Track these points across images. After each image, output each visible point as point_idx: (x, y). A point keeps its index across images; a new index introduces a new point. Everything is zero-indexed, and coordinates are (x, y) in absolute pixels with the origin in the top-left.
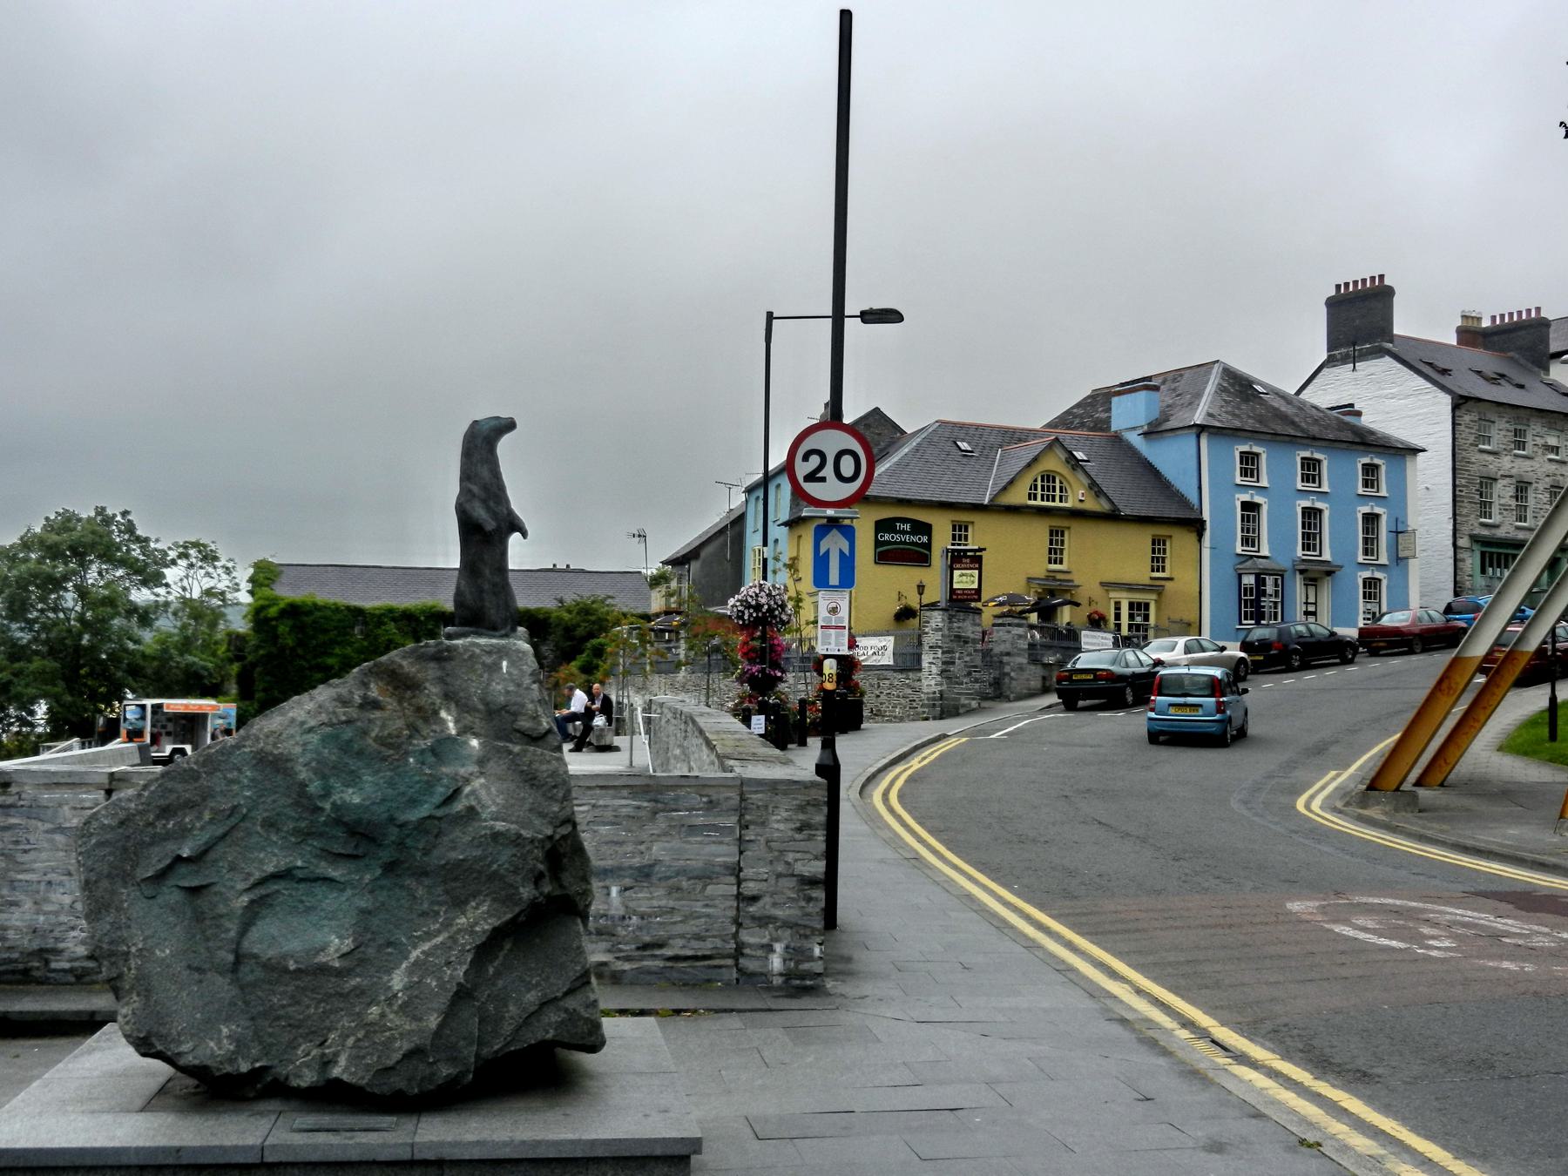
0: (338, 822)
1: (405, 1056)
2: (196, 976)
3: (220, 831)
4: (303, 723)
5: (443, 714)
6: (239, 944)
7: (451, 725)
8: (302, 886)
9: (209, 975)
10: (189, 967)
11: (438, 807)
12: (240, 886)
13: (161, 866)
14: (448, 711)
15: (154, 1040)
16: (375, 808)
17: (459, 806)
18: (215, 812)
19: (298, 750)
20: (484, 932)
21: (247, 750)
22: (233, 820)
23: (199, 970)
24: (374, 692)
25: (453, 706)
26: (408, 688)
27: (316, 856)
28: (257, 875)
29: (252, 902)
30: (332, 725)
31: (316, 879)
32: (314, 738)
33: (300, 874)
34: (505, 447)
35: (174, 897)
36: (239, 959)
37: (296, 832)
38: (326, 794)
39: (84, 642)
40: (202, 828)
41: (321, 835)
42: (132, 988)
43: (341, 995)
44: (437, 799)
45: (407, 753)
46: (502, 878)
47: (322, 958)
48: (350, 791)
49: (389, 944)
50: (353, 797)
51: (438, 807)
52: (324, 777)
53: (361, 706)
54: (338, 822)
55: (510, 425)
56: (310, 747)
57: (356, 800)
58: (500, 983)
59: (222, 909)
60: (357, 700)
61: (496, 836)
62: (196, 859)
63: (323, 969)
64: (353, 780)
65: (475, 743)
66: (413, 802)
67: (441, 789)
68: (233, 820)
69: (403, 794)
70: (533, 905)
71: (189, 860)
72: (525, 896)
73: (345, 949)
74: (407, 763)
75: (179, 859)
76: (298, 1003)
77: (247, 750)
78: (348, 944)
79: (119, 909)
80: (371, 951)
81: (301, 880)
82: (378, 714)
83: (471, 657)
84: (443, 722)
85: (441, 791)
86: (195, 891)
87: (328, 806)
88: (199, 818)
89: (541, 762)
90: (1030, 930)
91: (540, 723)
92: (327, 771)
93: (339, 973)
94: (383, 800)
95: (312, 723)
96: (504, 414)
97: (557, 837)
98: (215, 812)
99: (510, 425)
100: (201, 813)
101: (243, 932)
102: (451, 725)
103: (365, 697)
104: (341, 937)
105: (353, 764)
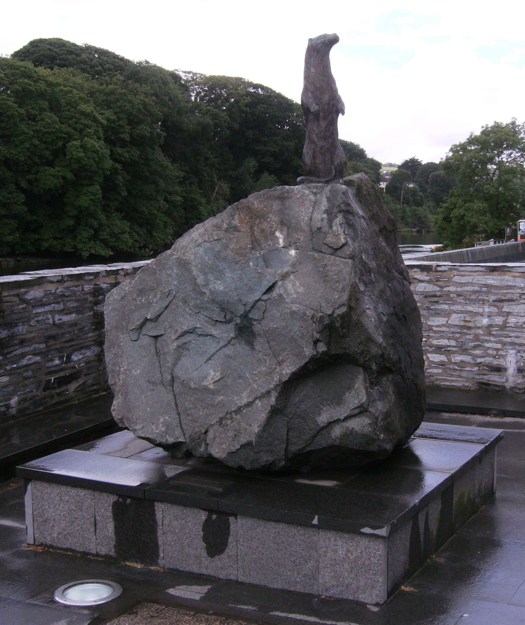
0: (213, 301)
1: (242, 446)
2: (151, 387)
3: (164, 306)
4: (196, 241)
5: (278, 234)
6: (173, 370)
7: (281, 241)
8: (201, 338)
9: (158, 387)
10: (149, 381)
11: (265, 293)
12: (174, 337)
13: (139, 323)
14: (281, 231)
15: (125, 421)
16: (230, 293)
17: (274, 294)
18: (163, 293)
19: (193, 257)
20: (287, 374)
21: (174, 257)
22: (170, 298)
23: (153, 383)
24: (236, 222)
25: (285, 229)
26: (258, 217)
27: (206, 322)
28: (180, 331)
29: (178, 346)
30: (210, 242)
31: (207, 335)
32: (201, 250)
33: (199, 331)
34: (336, 56)
35: (145, 341)
36: (173, 380)
37: (196, 306)
38: (207, 285)
39: (489, 166)
40: (156, 303)
41: (207, 308)
42: (119, 390)
43: (213, 405)
44: (264, 290)
45: (249, 259)
46: (296, 340)
47: (206, 383)
48: (219, 282)
49: (240, 377)
50: (219, 287)
51: (265, 293)
52: (205, 274)
53: (227, 230)
54: (213, 301)
55: (333, 40)
56: (198, 255)
57: (222, 288)
58: (303, 406)
59: (166, 350)
60: (225, 226)
61: (293, 313)
62: (156, 319)
63: (206, 389)
64: (220, 275)
65: (293, 252)
66: (251, 290)
67: (266, 283)
68: (170, 298)
69: (246, 285)
70: (313, 360)
71: (151, 320)
72: (307, 353)
73: (216, 379)
74: (249, 266)
75: (146, 320)
76: (196, 408)
77: (174, 257)
78: (218, 375)
79: (119, 346)
80: (229, 381)
81: (200, 335)
82: (236, 234)
83: (302, 196)
84: (277, 238)
85: (266, 284)
86: (156, 337)
87: (208, 292)
88: (155, 296)
89: (332, 265)
90: (455, 415)
91: (339, 239)
92: (206, 270)
93: (213, 393)
94: (236, 289)
95: (200, 241)
96: (330, 32)
97: (335, 315)
98: (163, 293)
99: (333, 40)
100: (156, 294)
101: (175, 364)
102: (281, 241)
103: (229, 224)
104: (214, 371)
105: (222, 265)
